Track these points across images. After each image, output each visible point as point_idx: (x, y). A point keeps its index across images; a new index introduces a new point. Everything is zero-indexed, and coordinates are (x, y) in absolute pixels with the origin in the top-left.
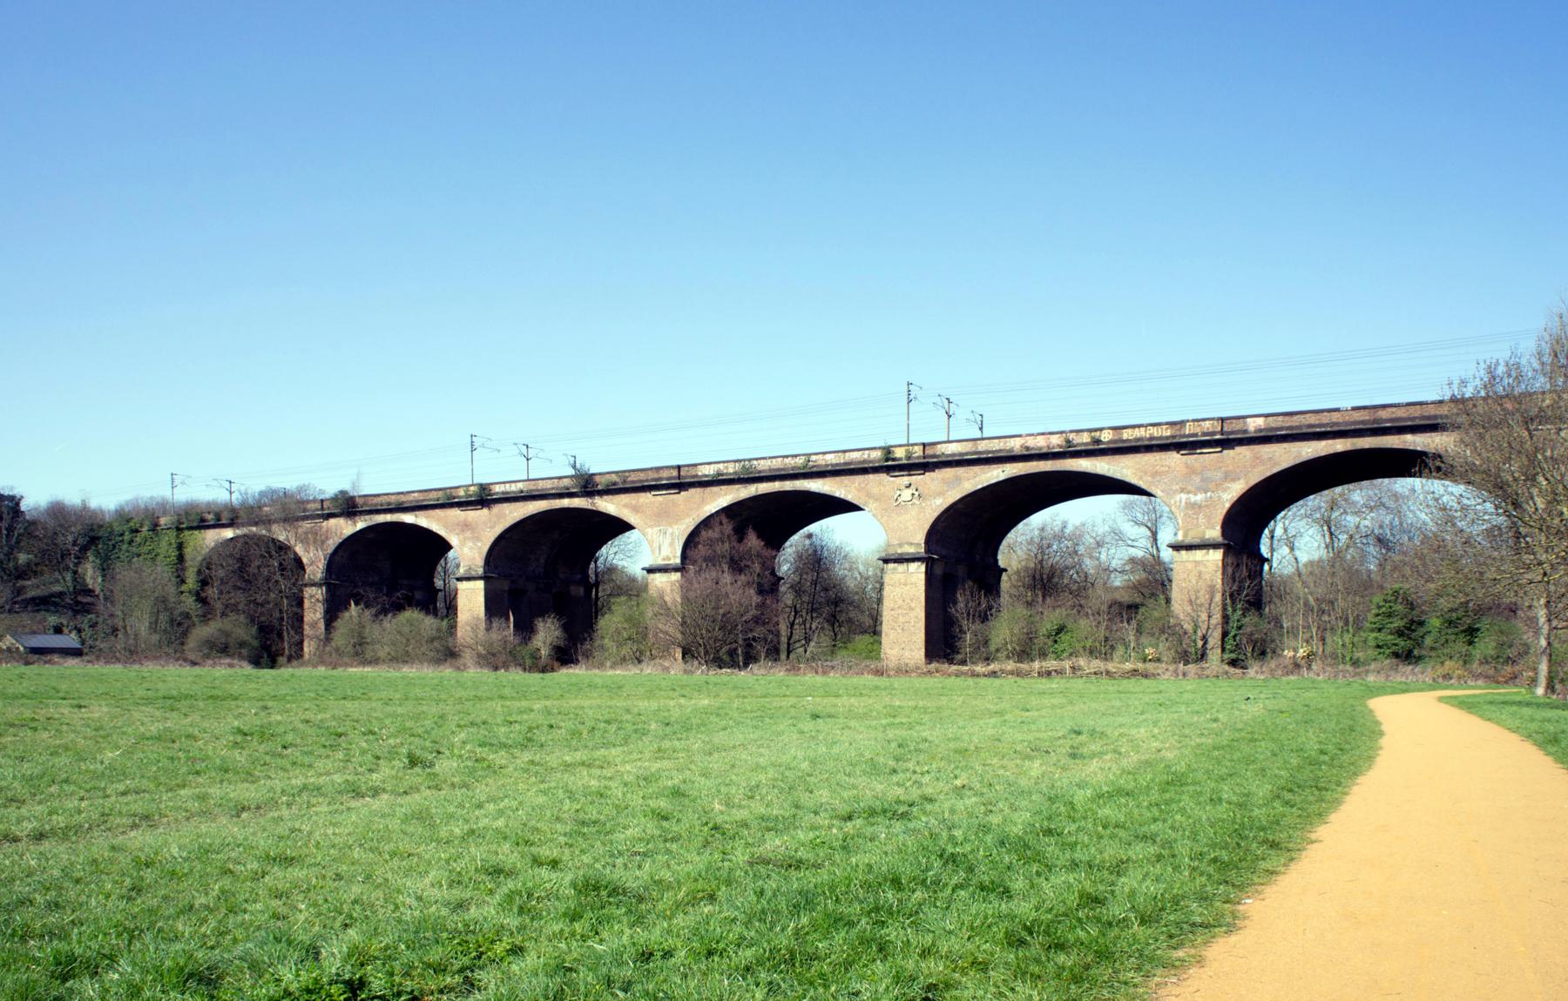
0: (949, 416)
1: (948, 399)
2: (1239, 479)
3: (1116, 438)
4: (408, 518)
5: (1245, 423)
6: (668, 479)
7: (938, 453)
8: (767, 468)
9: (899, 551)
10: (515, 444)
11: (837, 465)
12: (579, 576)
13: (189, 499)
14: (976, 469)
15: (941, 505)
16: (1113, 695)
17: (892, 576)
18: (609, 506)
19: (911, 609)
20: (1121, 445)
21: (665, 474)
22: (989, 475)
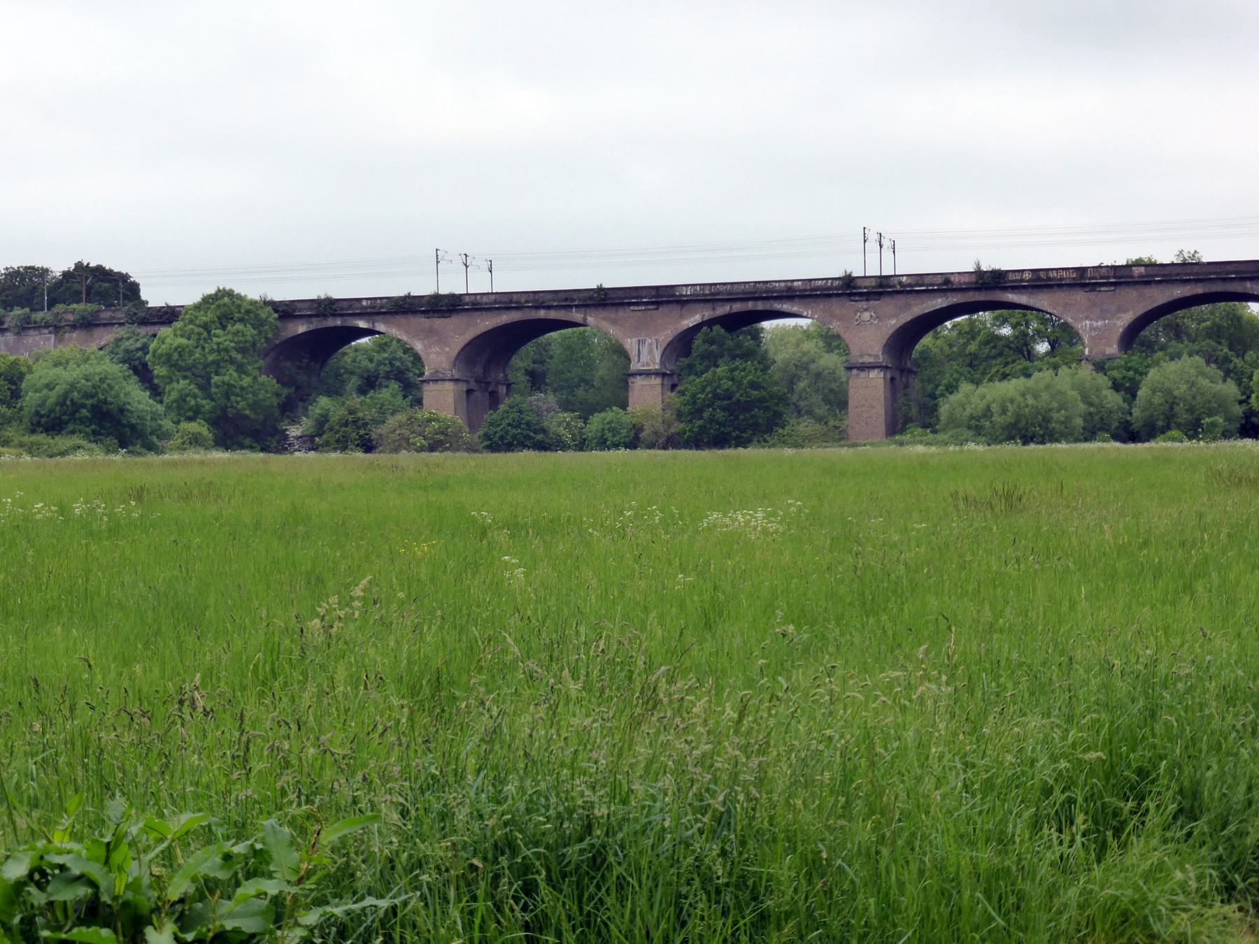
0: (467, 267)
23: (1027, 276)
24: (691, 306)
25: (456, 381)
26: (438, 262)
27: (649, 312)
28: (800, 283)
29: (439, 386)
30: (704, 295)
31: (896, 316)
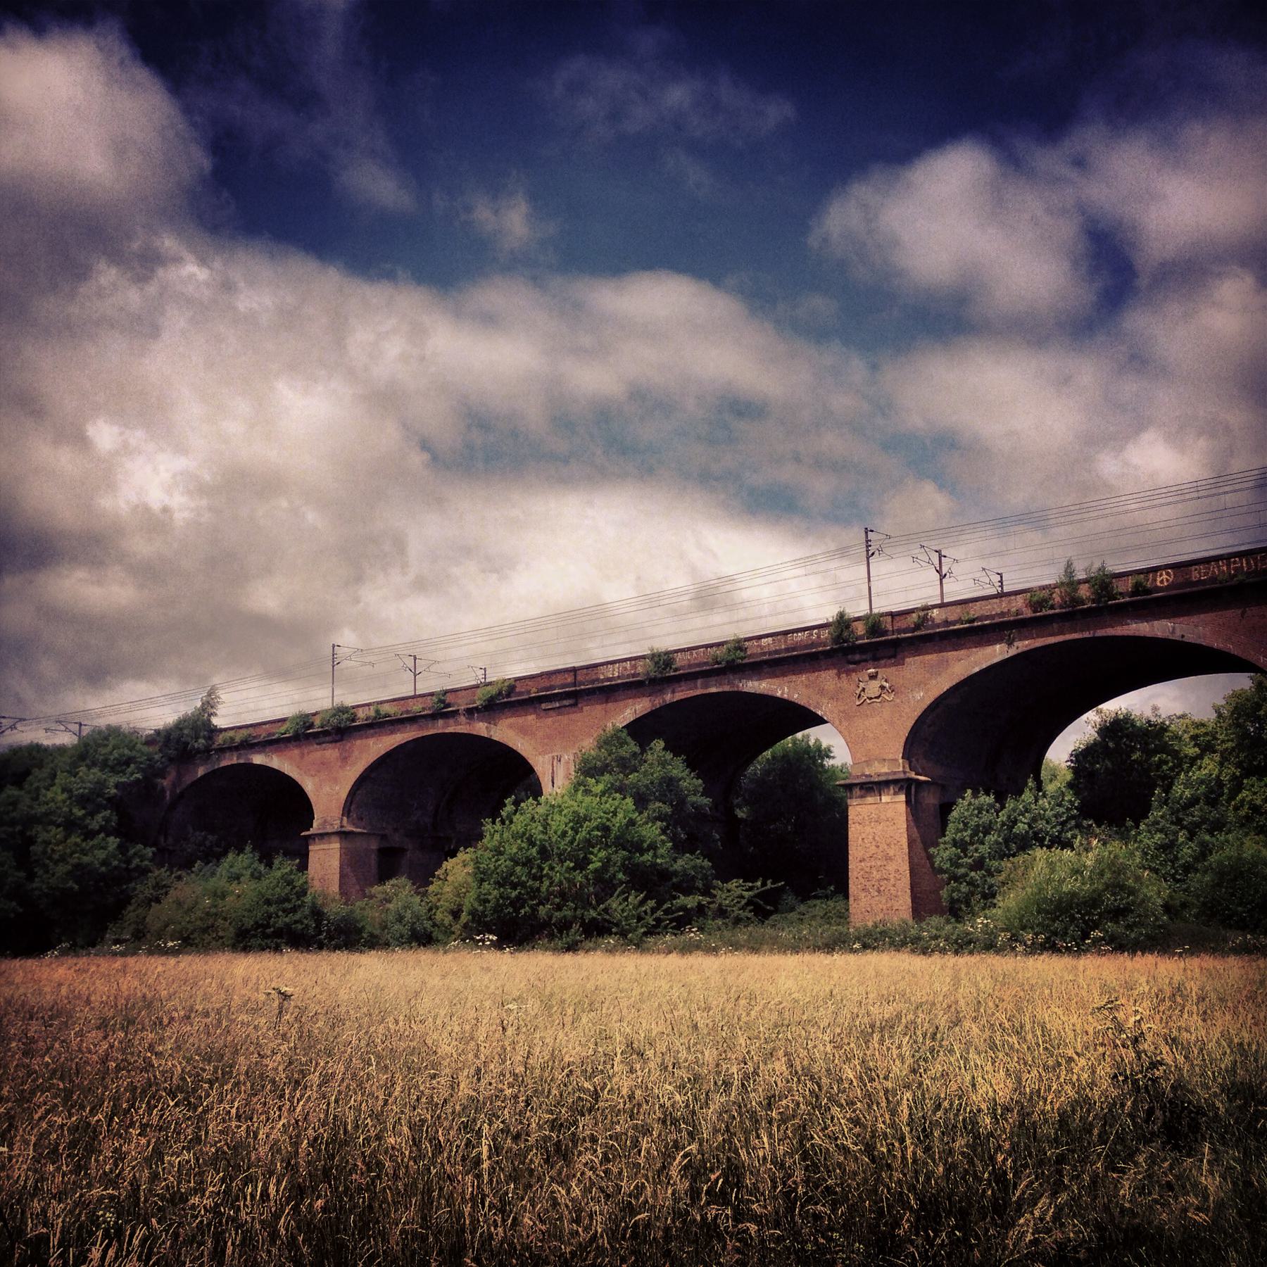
0: (942, 577)
3: (1180, 580)
4: (258, 759)
8: (686, 662)
10: (984, 569)
11: (776, 652)
13: (35, 741)
15: (923, 699)
18: (504, 732)
19: (889, 858)
21: (558, 681)
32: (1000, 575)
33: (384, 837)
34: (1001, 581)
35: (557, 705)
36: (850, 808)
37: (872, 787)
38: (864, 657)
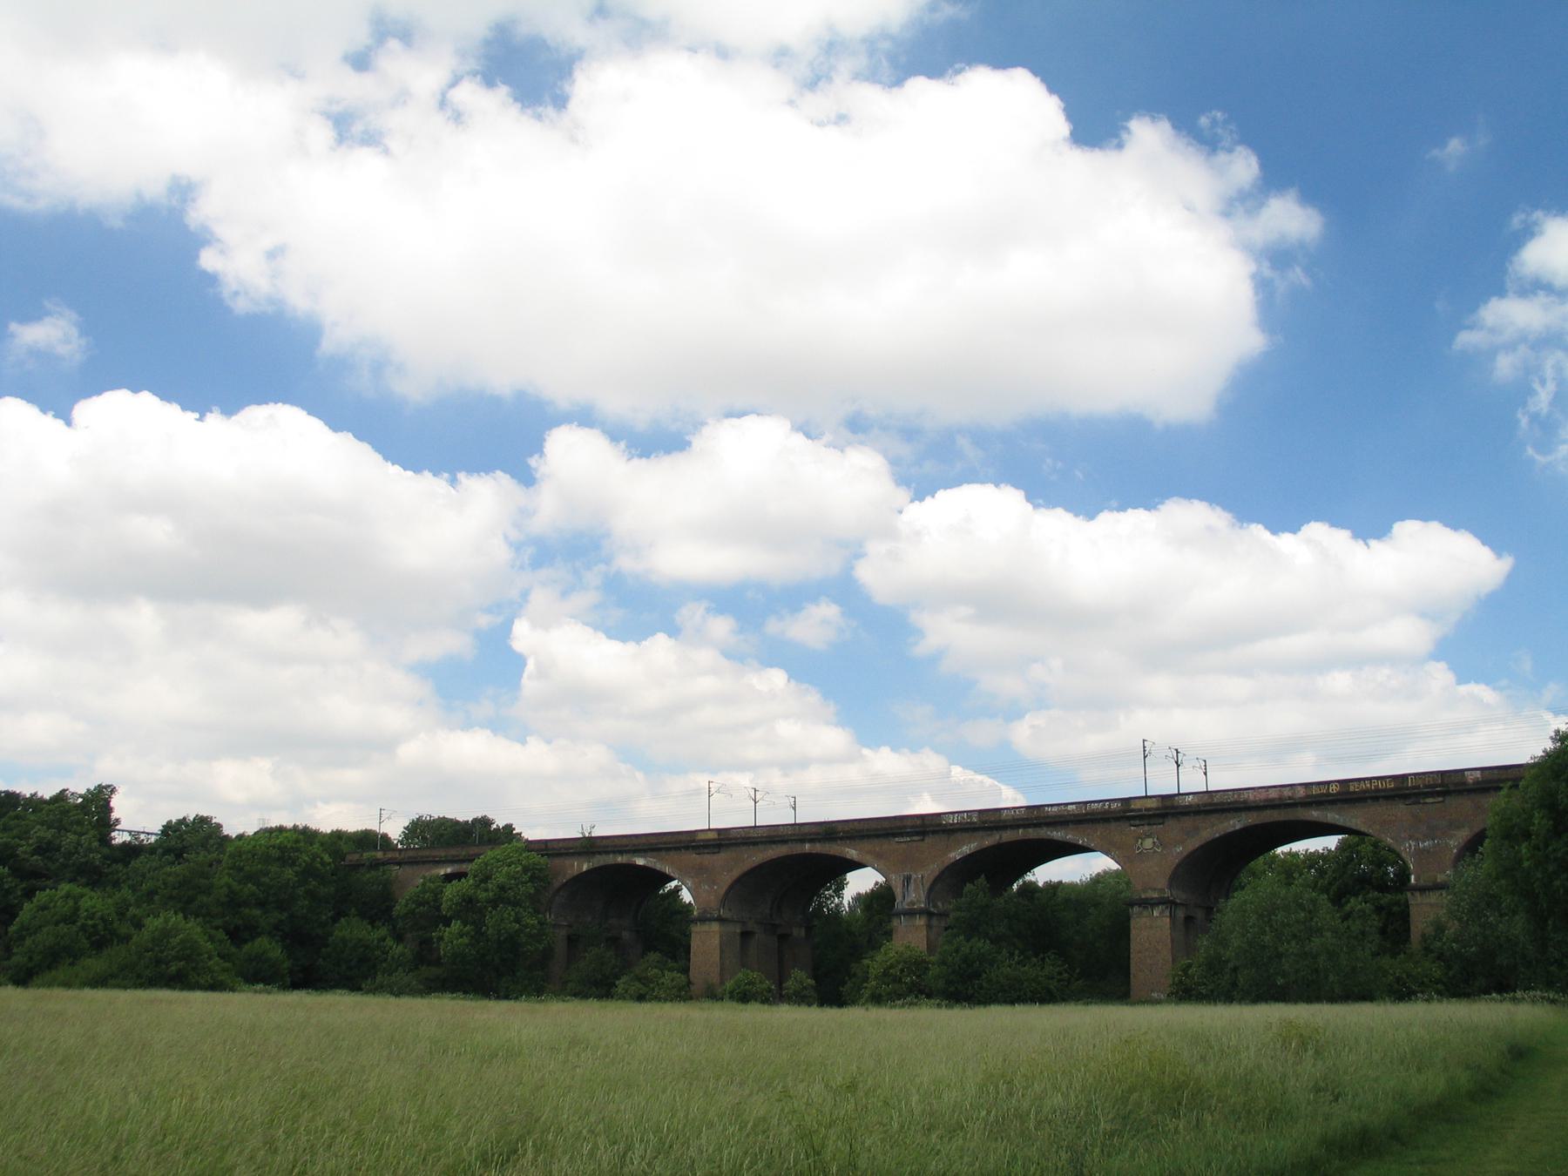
0: (1178, 766)
1: (1177, 750)
2: (1463, 827)
5: (1464, 775)
6: (912, 827)
7: (1176, 804)
9: (1143, 896)
12: (422, 880)
14: (1213, 818)
16: (967, 1144)
17: (1138, 920)
20: (1349, 797)
22: (1226, 824)
23: (1334, 789)
24: (959, 836)
25: (720, 920)
26: (1145, 757)
27: (914, 844)
28: (1074, 807)
29: (705, 927)
30: (971, 823)
31: (1183, 842)
32: (1205, 761)
33: (744, 923)
34: (1205, 766)
35: (908, 839)
36: (1132, 919)
37: (1147, 904)
38: (1142, 823)
